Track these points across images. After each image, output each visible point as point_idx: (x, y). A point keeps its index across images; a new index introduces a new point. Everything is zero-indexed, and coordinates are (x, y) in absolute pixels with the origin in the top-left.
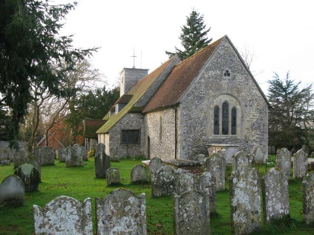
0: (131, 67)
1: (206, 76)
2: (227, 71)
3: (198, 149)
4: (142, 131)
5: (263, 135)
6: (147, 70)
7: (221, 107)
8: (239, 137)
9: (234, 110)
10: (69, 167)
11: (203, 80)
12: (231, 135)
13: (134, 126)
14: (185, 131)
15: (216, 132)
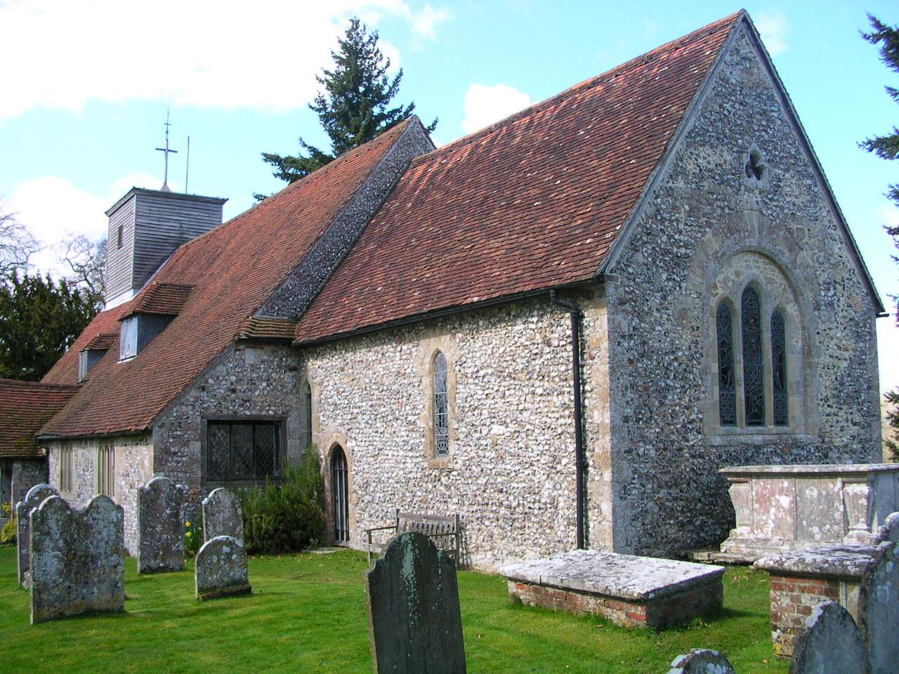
0: (157, 187)
1: (691, 167)
2: (754, 158)
3: (674, 492)
4: (292, 424)
5: (869, 426)
6: (220, 202)
7: (738, 306)
8: (801, 436)
9: (779, 320)
10: (46, 620)
11: (681, 184)
12: (771, 427)
13: (262, 404)
14: (629, 411)
15: (728, 418)
